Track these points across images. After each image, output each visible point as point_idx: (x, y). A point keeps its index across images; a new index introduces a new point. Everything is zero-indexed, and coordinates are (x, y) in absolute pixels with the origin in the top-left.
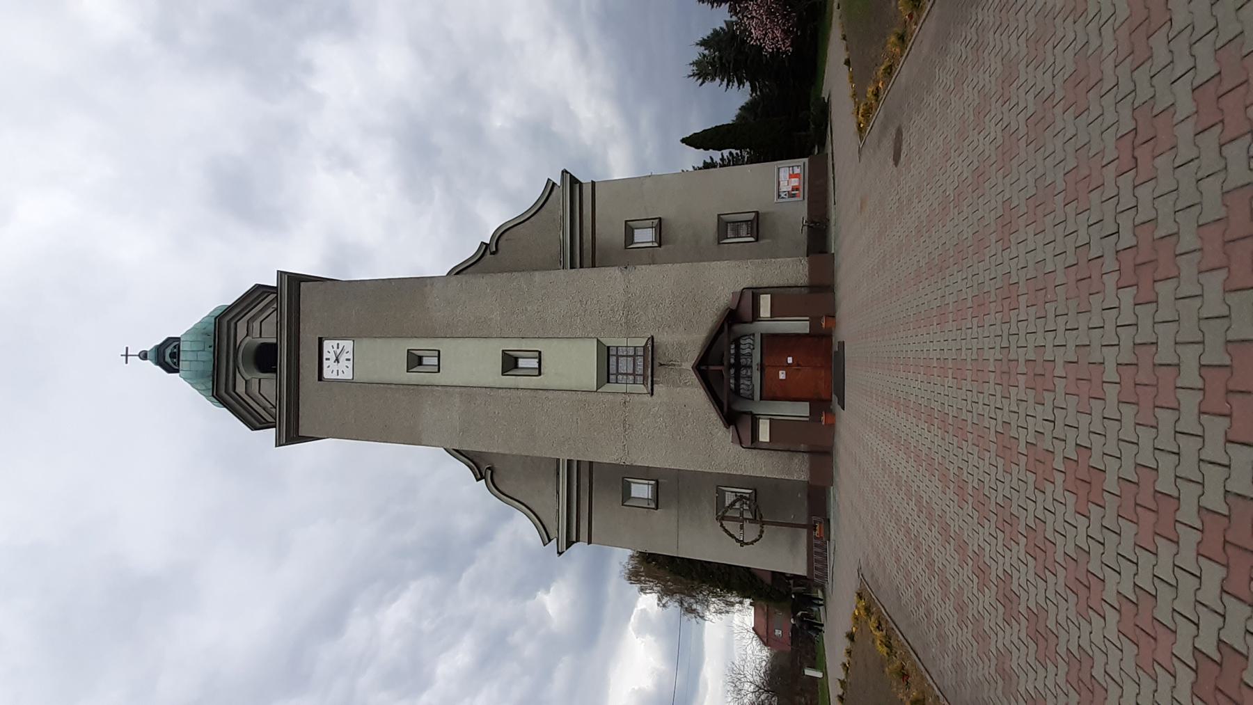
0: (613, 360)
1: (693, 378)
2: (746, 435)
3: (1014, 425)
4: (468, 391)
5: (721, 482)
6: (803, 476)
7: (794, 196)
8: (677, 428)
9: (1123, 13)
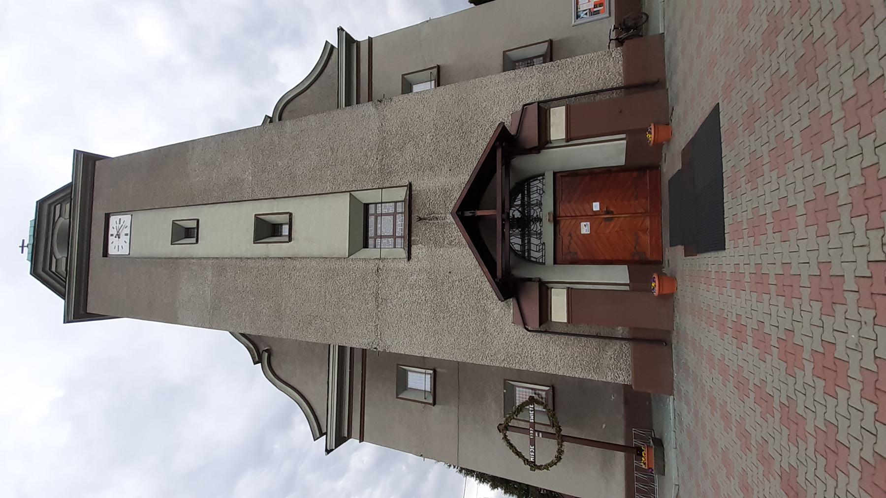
0: (371, 220)
1: (456, 232)
2: (532, 311)
3: (767, 324)
4: (221, 264)
5: (509, 380)
6: (624, 377)
7: (597, 13)
8: (440, 302)
9: (839, 9)
